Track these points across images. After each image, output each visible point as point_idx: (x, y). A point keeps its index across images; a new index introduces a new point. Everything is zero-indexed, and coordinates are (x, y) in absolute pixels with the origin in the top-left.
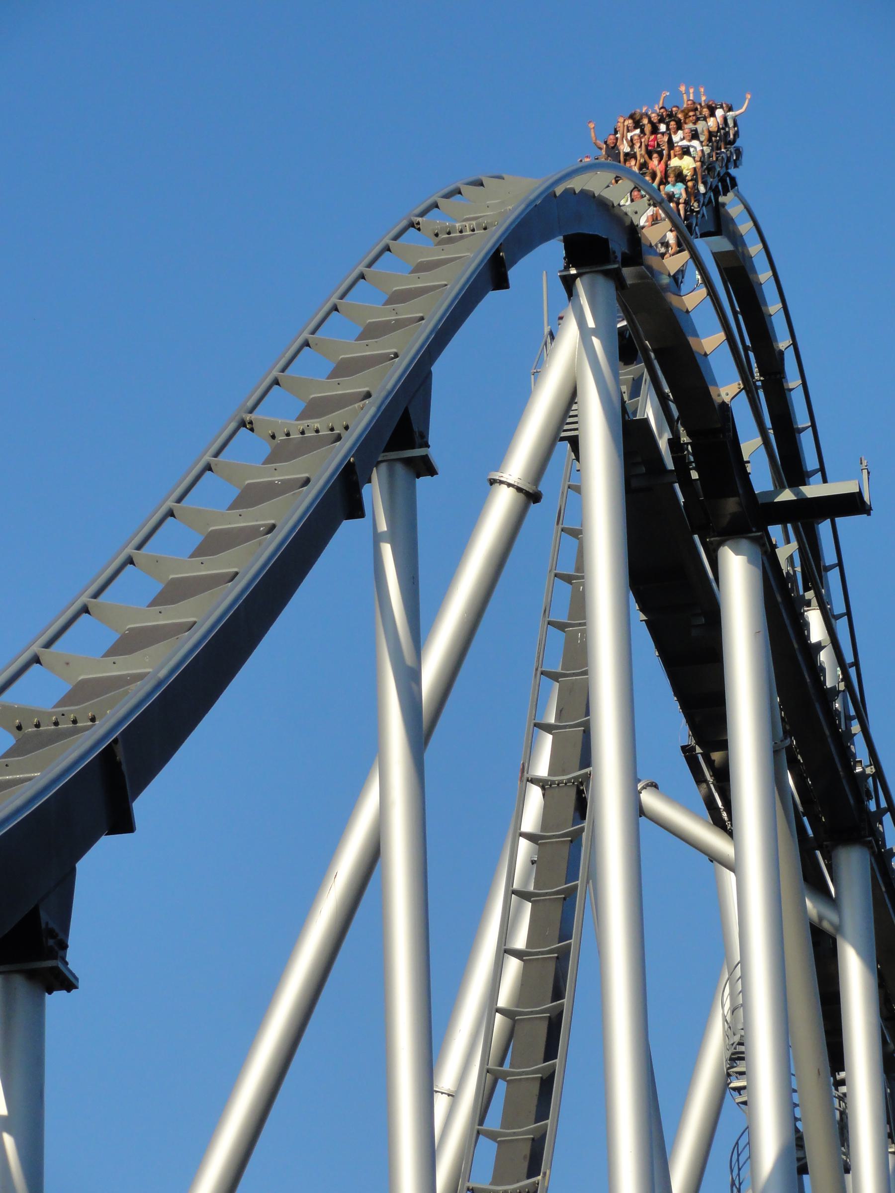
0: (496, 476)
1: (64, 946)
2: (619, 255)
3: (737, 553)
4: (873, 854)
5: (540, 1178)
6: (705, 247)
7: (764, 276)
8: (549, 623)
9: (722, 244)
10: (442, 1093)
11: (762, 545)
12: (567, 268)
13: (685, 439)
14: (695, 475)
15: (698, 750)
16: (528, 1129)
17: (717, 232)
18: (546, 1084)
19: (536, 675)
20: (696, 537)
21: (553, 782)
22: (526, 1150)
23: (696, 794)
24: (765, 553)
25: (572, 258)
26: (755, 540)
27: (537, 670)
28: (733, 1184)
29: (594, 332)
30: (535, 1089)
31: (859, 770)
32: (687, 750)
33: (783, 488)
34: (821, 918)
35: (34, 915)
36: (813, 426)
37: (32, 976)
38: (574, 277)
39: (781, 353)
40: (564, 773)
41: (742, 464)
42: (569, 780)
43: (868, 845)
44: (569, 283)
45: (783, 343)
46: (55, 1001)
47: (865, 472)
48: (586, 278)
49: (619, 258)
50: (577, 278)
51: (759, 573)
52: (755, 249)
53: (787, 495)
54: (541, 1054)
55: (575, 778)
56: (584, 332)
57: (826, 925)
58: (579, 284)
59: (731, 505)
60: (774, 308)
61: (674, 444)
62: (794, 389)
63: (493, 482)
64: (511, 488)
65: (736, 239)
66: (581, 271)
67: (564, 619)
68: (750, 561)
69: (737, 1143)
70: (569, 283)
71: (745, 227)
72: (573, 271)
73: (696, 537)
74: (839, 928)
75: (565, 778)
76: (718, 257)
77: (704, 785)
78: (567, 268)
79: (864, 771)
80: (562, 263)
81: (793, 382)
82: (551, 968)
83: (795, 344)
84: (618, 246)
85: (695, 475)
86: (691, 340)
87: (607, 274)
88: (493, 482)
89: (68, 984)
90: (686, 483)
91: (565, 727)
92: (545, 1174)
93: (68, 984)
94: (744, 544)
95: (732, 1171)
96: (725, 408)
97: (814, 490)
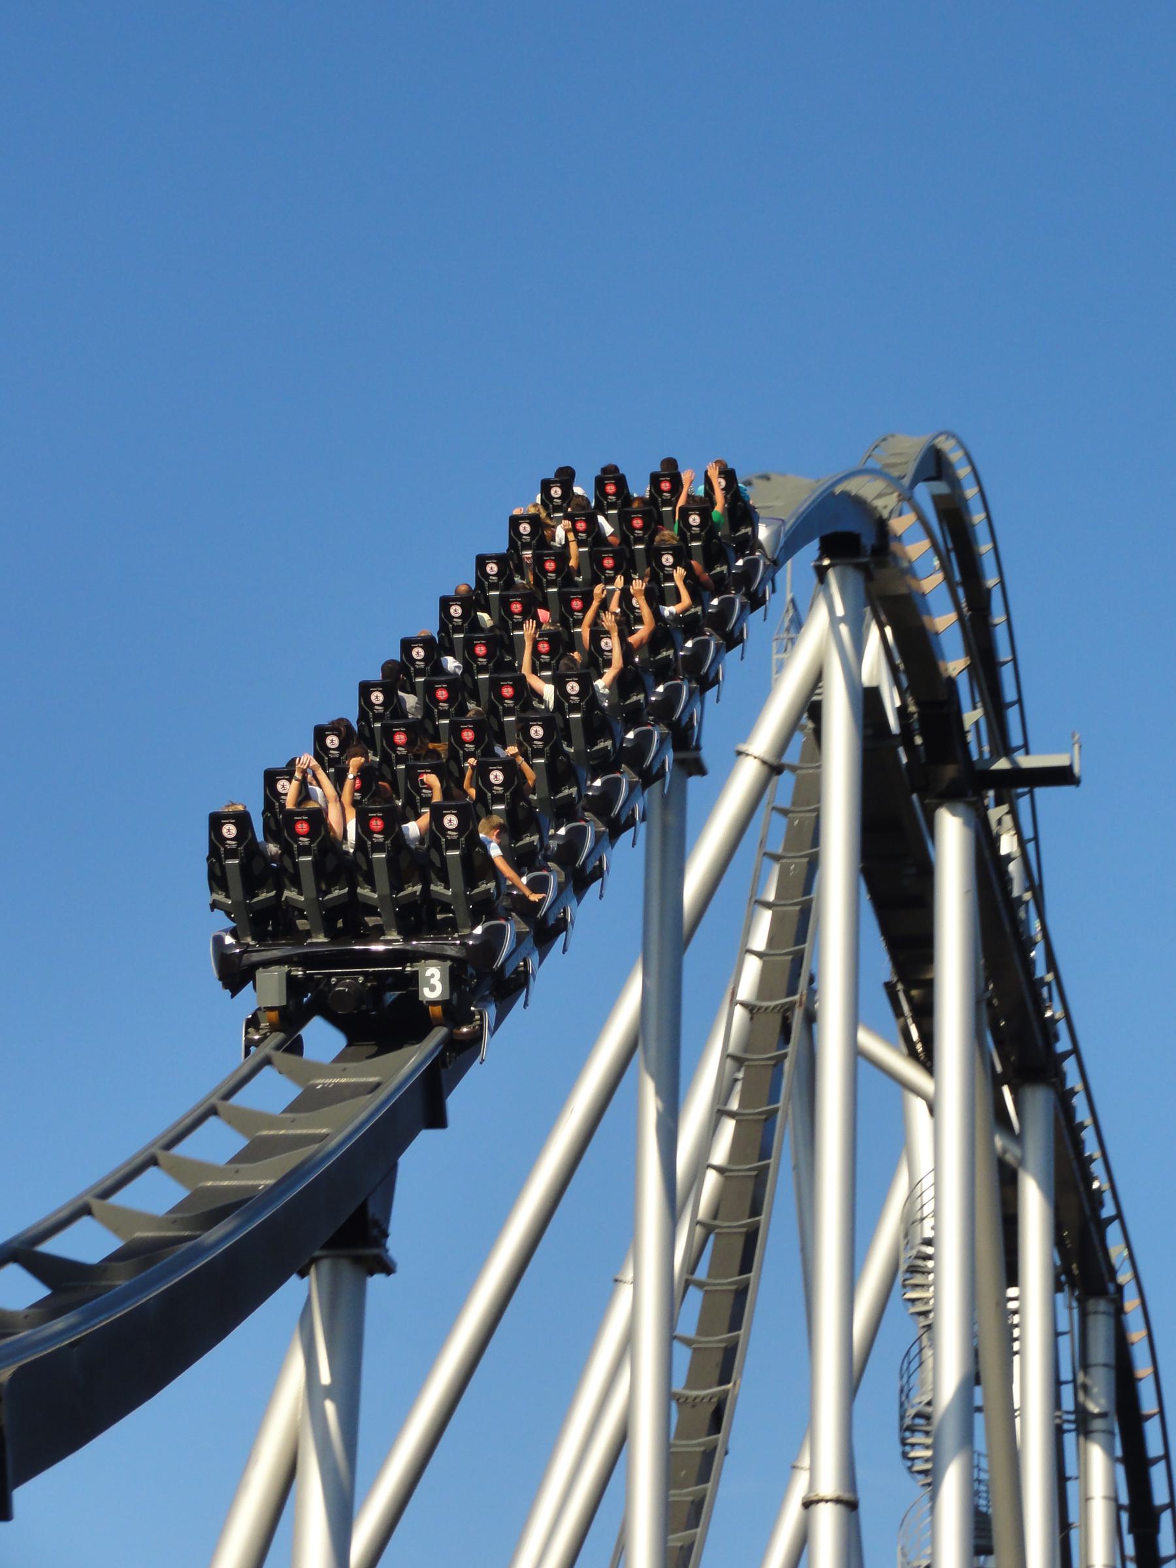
0: (743, 748)
1: (385, 1235)
2: (869, 549)
3: (954, 814)
4: (1057, 1093)
5: (731, 1385)
6: (923, 493)
7: (978, 517)
8: (765, 854)
9: (942, 488)
10: (827, 1501)
11: (977, 810)
12: (821, 558)
13: (912, 708)
14: (918, 740)
15: (900, 987)
16: (719, 1339)
17: (937, 477)
18: (741, 1295)
19: (749, 904)
20: (915, 797)
21: (760, 1008)
22: (718, 1357)
23: (894, 1026)
24: (978, 816)
25: (825, 551)
26: (970, 804)
27: (751, 897)
28: (902, 1391)
29: (843, 620)
30: (729, 1300)
31: (1048, 1014)
32: (890, 988)
33: (999, 758)
34: (1005, 1151)
35: (363, 1208)
36: (1015, 660)
37: (357, 1261)
38: (827, 567)
39: (989, 591)
40: (771, 999)
41: (963, 734)
42: (775, 1007)
43: (1053, 1085)
44: (821, 573)
45: (991, 581)
46: (376, 1283)
47: (1076, 747)
48: (838, 568)
49: (869, 552)
50: (828, 569)
51: (971, 834)
52: (971, 492)
53: (1002, 764)
54: (737, 1268)
55: (783, 1005)
56: (834, 621)
57: (1009, 1158)
58: (832, 576)
59: (950, 771)
60: (985, 548)
61: (902, 712)
62: (999, 624)
63: (740, 753)
64: (756, 760)
65: (955, 483)
66: (835, 562)
67: (779, 851)
68: (967, 823)
69: (908, 1353)
70: (821, 573)
71: (963, 472)
72: (826, 562)
73: (915, 797)
74: (1022, 1162)
75: (773, 1003)
76: (937, 500)
77: (902, 1020)
78: (821, 558)
79: (1053, 1016)
80: (817, 554)
81: (998, 618)
82: (750, 1186)
83: (1002, 583)
84: (868, 540)
85: (918, 740)
86: (925, 619)
87: (857, 566)
88: (740, 753)
89: (387, 1268)
90: (911, 749)
91: (772, 955)
92: (735, 1384)
93: (387, 1268)
94: (961, 807)
95: (902, 1377)
96: (951, 683)
97: (1026, 762)
